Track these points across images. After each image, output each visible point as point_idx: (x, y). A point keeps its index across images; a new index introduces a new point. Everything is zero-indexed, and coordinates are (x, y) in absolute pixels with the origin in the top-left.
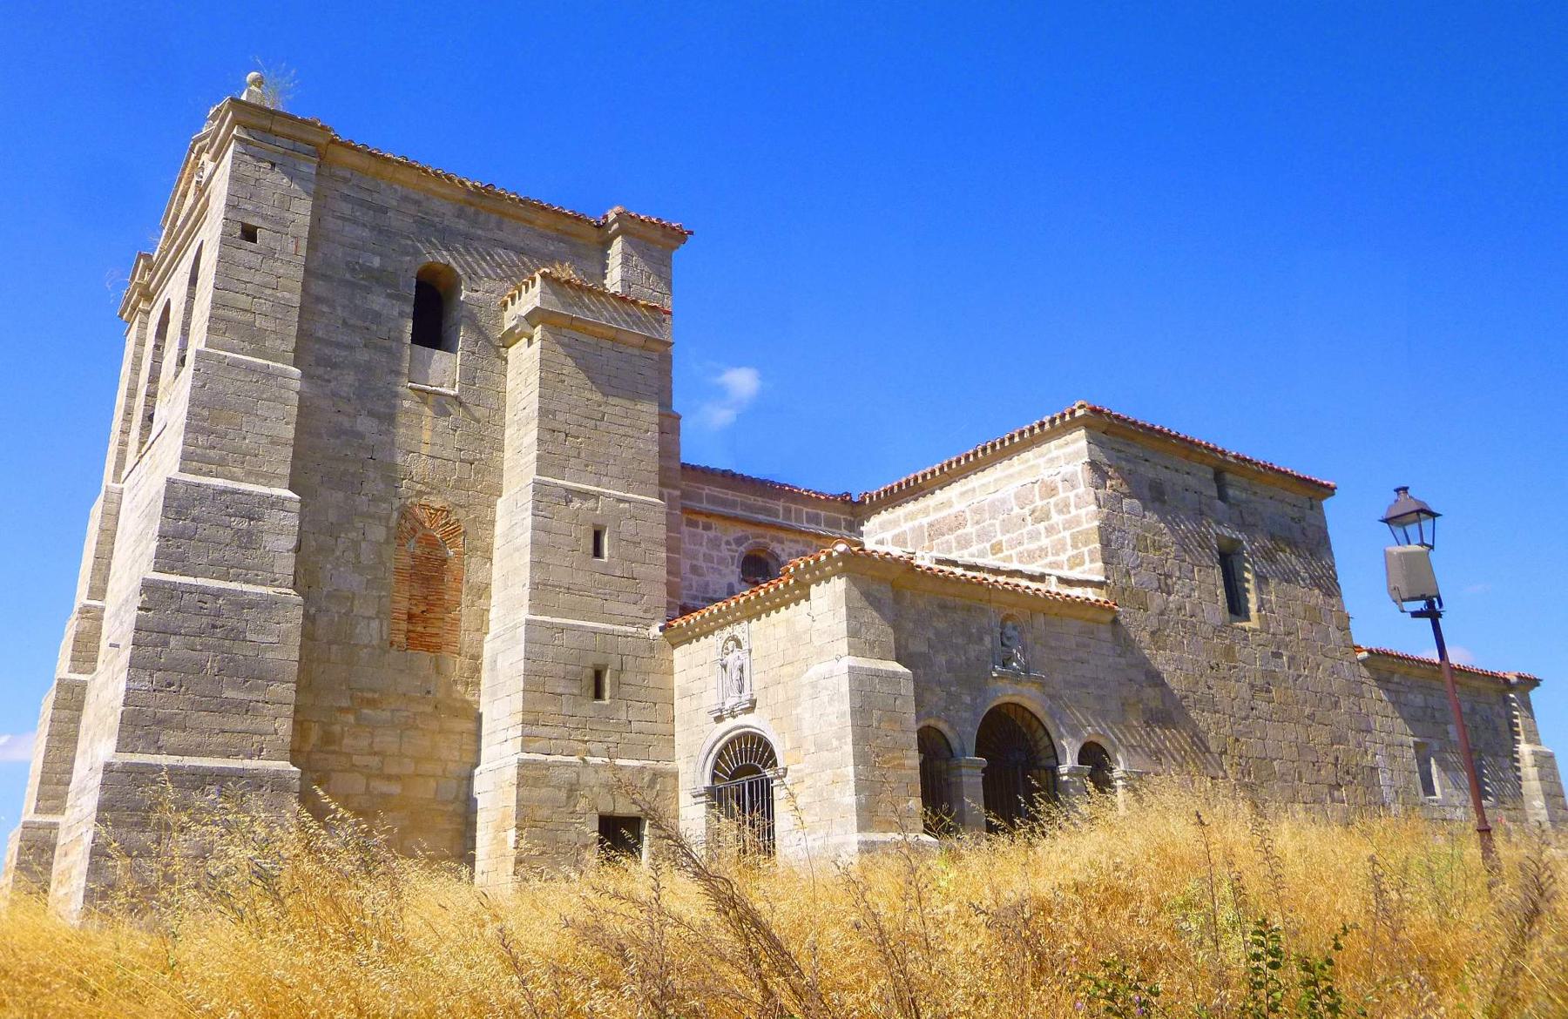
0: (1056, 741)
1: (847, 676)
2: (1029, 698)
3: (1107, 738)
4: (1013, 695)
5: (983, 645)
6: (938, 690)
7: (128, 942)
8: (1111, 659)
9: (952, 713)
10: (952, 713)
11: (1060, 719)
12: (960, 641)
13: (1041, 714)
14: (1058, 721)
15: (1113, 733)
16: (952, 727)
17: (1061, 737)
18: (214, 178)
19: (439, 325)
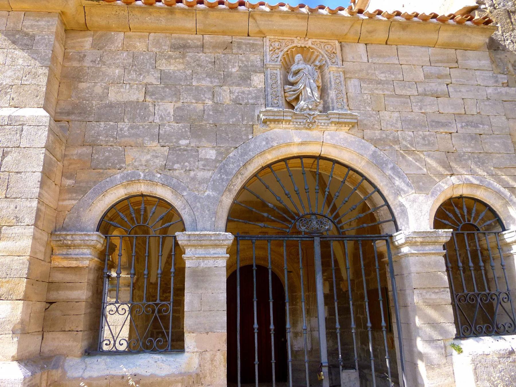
0: (390, 199)
1: (225, 268)
2: (335, 146)
3: (488, 188)
4: (302, 144)
5: (250, 85)
6: (154, 145)
7: (9, 92)
8: (490, 90)
9: (176, 173)
10: (176, 173)
11: (393, 168)
12: (206, 83)
13: (360, 165)
14: (389, 172)
15: (500, 181)
16: (175, 189)
17: (398, 192)
18: (120, 204)
19: (285, 318)
